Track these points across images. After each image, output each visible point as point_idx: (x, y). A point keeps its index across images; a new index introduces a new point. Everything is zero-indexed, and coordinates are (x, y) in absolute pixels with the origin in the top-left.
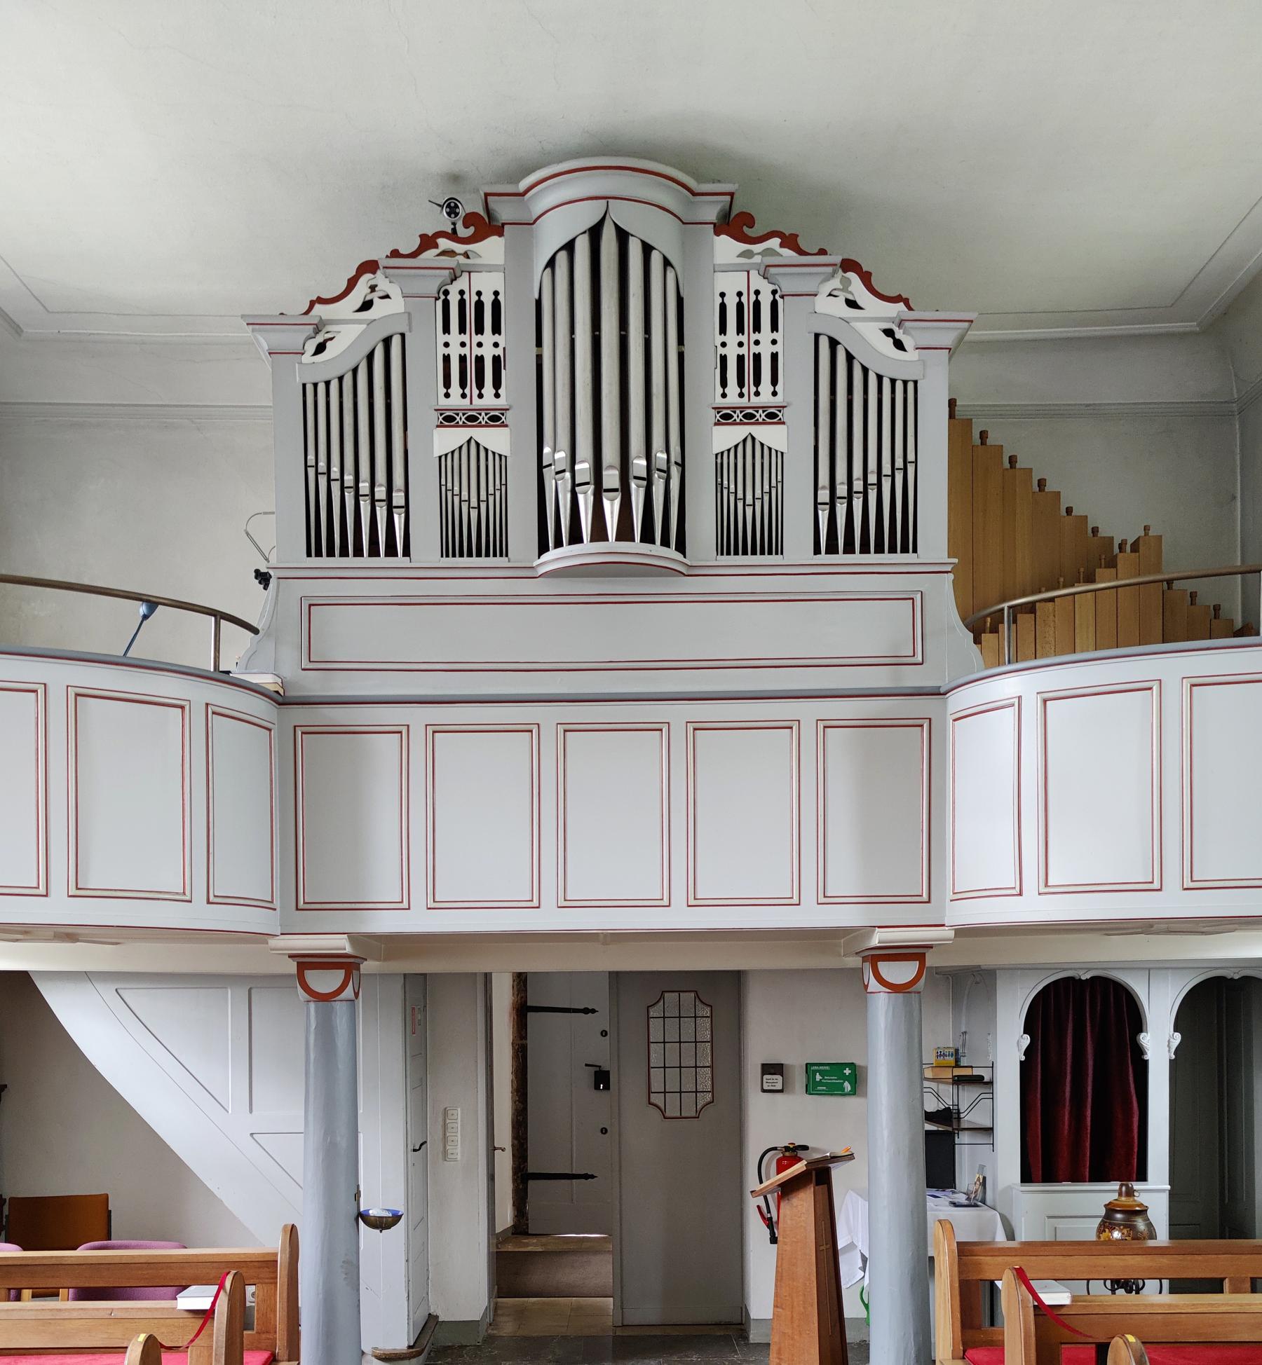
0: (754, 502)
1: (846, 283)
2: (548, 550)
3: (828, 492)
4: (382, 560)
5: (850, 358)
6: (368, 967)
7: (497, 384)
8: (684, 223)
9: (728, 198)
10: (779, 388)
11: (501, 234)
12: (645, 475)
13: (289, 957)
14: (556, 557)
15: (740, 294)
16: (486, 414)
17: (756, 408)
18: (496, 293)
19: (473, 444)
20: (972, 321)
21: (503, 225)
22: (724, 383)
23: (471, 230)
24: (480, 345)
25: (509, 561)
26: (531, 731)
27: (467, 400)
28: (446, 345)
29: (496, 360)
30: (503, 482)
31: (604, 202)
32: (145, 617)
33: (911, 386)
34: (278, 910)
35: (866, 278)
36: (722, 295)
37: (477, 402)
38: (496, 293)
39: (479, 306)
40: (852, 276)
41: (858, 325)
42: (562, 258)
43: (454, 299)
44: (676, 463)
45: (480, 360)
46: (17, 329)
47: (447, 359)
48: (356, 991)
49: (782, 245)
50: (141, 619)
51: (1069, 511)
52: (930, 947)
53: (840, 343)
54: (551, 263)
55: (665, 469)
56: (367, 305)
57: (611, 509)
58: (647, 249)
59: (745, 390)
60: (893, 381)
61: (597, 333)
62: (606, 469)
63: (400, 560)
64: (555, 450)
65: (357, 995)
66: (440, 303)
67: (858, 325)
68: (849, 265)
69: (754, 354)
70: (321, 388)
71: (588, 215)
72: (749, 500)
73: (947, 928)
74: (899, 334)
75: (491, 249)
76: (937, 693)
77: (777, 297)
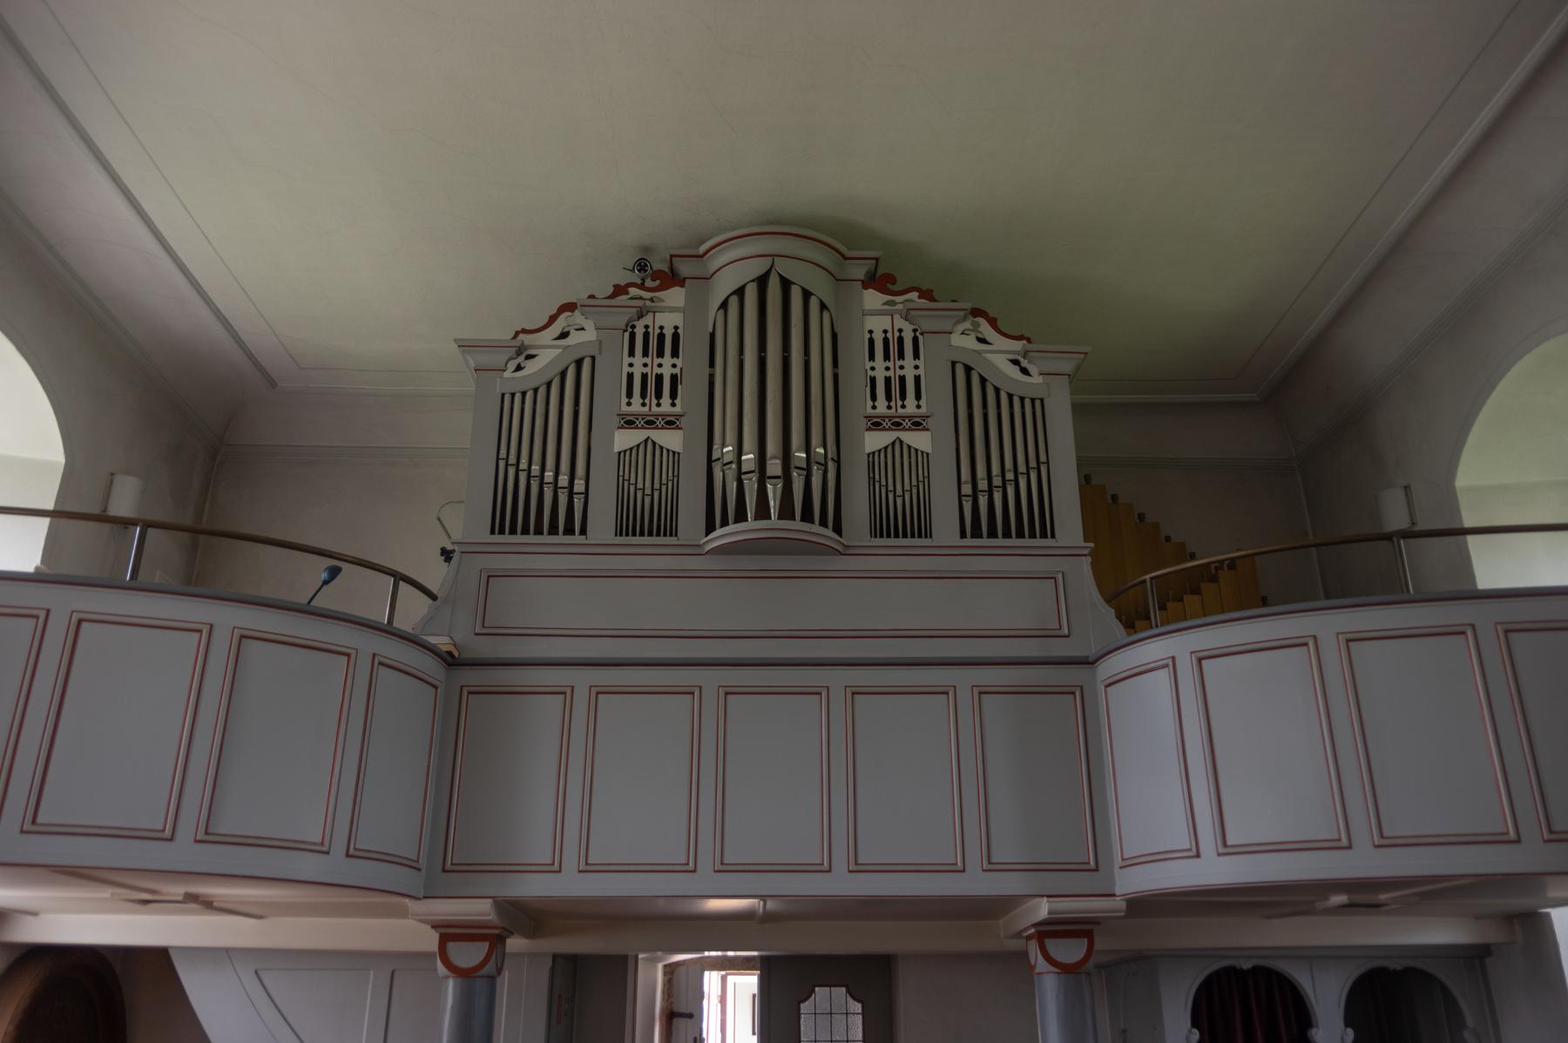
0: (904, 494)
1: (976, 326)
2: (715, 530)
3: (970, 486)
4: (561, 538)
5: (983, 380)
6: (515, 944)
7: (673, 395)
8: (837, 280)
9: (874, 262)
10: (923, 402)
11: (682, 285)
12: (804, 466)
13: (433, 927)
14: (725, 535)
15: (885, 332)
16: (663, 420)
17: (903, 417)
18: (676, 328)
19: (650, 444)
20: (1086, 353)
21: (685, 279)
22: (874, 398)
23: (658, 282)
24: (660, 365)
25: (678, 539)
26: (693, 693)
27: (647, 409)
28: (631, 365)
29: (674, 378)
30: (676, 474)
31: (770, 259)
32: (326, 583)
33: (1038, 403)
34: (423, 871)
35: (993, 323)
36: (871, 332)
37: (655, 409)
38: (676, 328)
39: (661, 337)
40: (981, 320)
41: (989, 356)
42: (734, 301)
43: (639, 332)
44: (832, 459)
45: (659, 378)
46: (272, 383)
47: (630, 376)
48: (499, 966)
49: (920, 297)
50: (321, 583)
51: (1168, 539)
52: (1098, 923)
53: (973, 369)
54: (724, 305)
55: (823, 462)
56: (564, 335)
57: (773, 492)
58: (807, 295)
59: (893, 404)
60: (1022, 399)
61: (763, 354)
62: (770, 459)
63: (577, 538)
64: (724, 445)
65: (499, 971)
66: (627, 335)
67: (989, 356)
68: (976, 312)
69: (900, 376)
70: (518, 397)
71: (757, 268)
72: (899, 491)
73: (1118, 898)
74: (1024, 363)
75: (675, 296)
76: (1088, 662)
77: (918, 334)
